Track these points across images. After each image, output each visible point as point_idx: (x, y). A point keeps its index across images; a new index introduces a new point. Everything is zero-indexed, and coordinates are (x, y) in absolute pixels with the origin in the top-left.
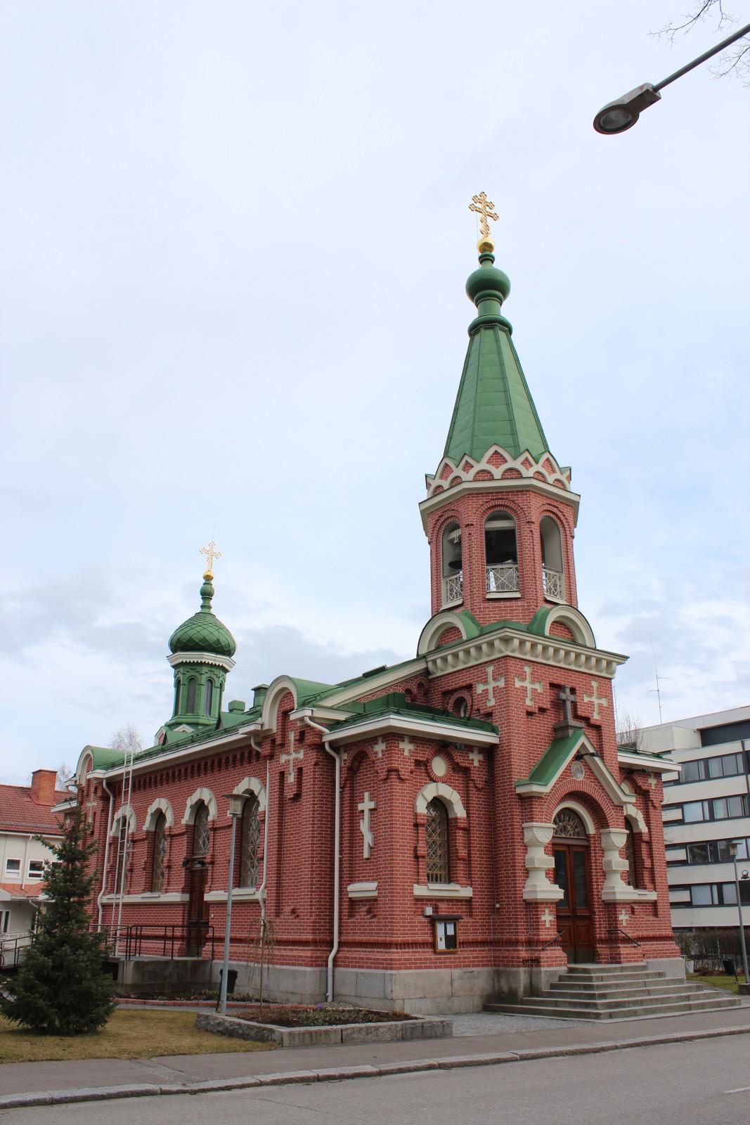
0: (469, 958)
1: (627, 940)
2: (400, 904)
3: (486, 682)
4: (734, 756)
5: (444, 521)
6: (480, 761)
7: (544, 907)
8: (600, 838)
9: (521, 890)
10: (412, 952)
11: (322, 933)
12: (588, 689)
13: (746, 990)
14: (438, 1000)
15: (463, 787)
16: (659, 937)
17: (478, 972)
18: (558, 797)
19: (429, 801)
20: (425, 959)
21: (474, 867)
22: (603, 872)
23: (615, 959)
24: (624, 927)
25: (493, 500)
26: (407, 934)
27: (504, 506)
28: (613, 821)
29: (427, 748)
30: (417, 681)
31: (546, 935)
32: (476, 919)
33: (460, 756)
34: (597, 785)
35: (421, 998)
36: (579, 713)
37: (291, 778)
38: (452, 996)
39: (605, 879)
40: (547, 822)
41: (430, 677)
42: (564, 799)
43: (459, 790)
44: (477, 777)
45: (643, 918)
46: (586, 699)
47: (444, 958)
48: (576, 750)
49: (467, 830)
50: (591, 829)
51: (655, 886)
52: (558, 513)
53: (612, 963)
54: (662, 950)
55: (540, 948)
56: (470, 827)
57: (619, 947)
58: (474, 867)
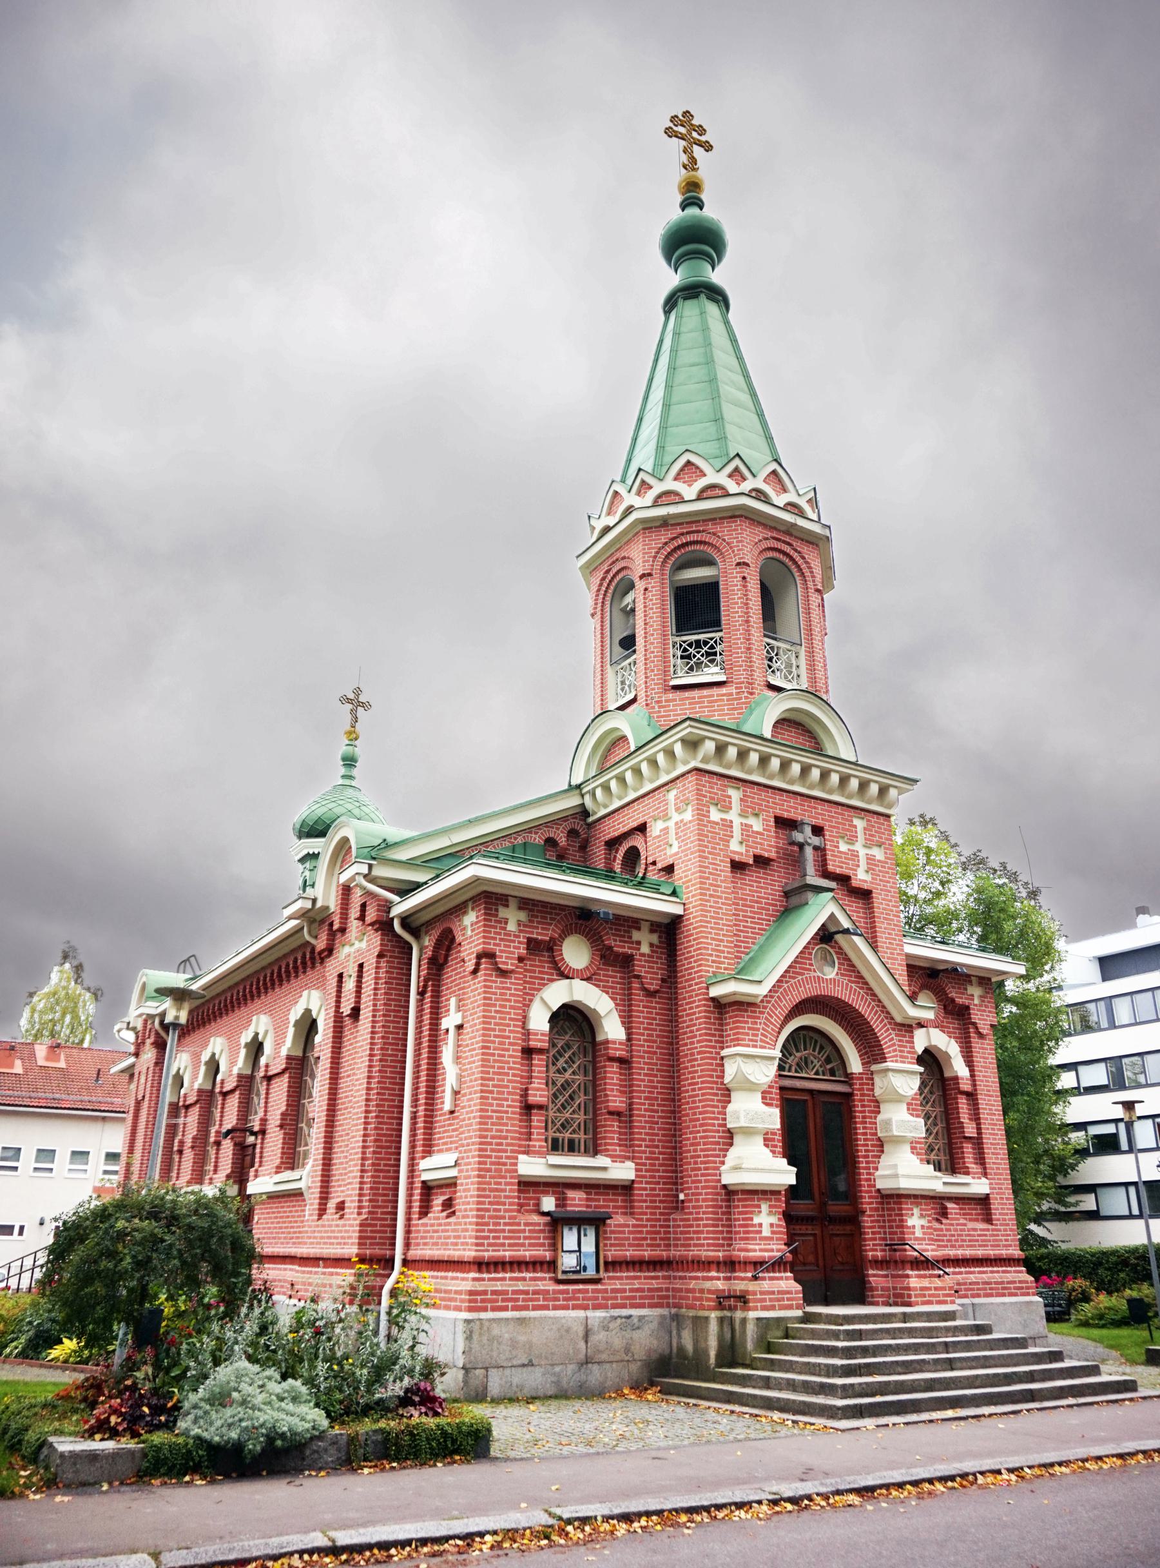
0: (624, 1291)
1: (921, 1263)
2: (491, 1190)
3: (666, 817)
4: (1150, 994)
5: (612, 578)
6: (651, 945)
7: (759, 1200)
8: (872, 1079)
9: (718, 1168)
10: (511, 1279)
11: (378, 1244)
12: (848, 830)
13: (1156, 1359)
14: (557, 1369)
15: (623, 989)
16: (995, 1260)
17: (641, 1318)
18: (787, 1005)
19: (555, 1009)
20: (535, 1292)
21: (638, 1127)
22: (879, 1139)
23: (900, 1297)
24: (917, 1239)
25: (682, 534)
26: (503, 1245)
27: (701, 542)
28: (895, 1050)
29: (551, 919)
30: (567, 826)
31: (761, 1250)
32: (641, 1220)
33: (614, 935)
34: (861, 988)
35: (524, 1365)
36: (830, 868)
37: (350, 985)
38: (587, 1363)
39: (882, 1151)
40: (764, 1047)
41: (590, 819)
42: (800, 1008)
43: (613, 993)
44: (646, 972)
45: (965, 1225)
46: (843, 847)
47: (574, 1291)
48: (819, 926)
49: (624, 1062)
50: (855, 1065)
51: (985, 1168)
52: (792, 553)
53: (896, 1304)
54: (1002, 1283)
55: (749, 1275)
56: (632, 1056)
57: (908, 1276)
58: (638, 1127)
